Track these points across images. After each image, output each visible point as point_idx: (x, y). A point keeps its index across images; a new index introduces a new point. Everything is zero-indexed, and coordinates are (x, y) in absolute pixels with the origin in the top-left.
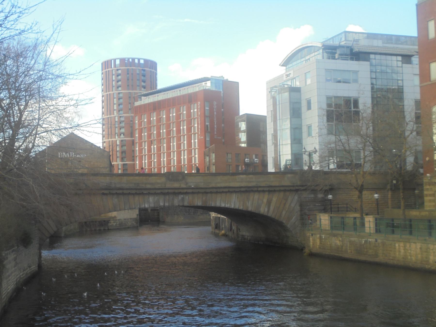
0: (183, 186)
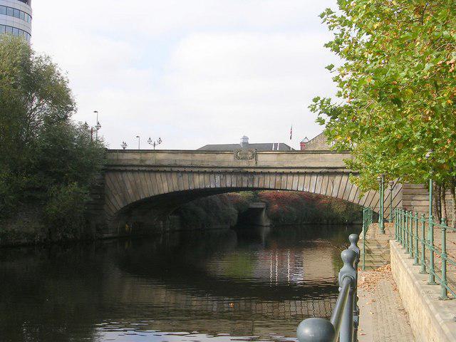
0: (253, 164)
